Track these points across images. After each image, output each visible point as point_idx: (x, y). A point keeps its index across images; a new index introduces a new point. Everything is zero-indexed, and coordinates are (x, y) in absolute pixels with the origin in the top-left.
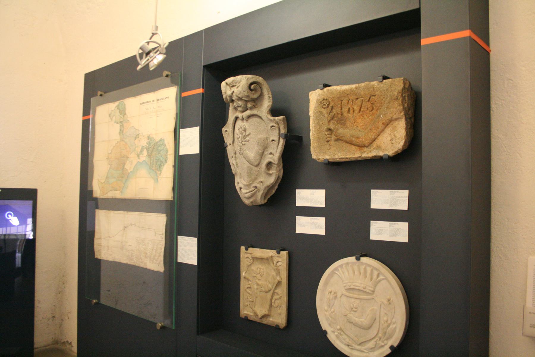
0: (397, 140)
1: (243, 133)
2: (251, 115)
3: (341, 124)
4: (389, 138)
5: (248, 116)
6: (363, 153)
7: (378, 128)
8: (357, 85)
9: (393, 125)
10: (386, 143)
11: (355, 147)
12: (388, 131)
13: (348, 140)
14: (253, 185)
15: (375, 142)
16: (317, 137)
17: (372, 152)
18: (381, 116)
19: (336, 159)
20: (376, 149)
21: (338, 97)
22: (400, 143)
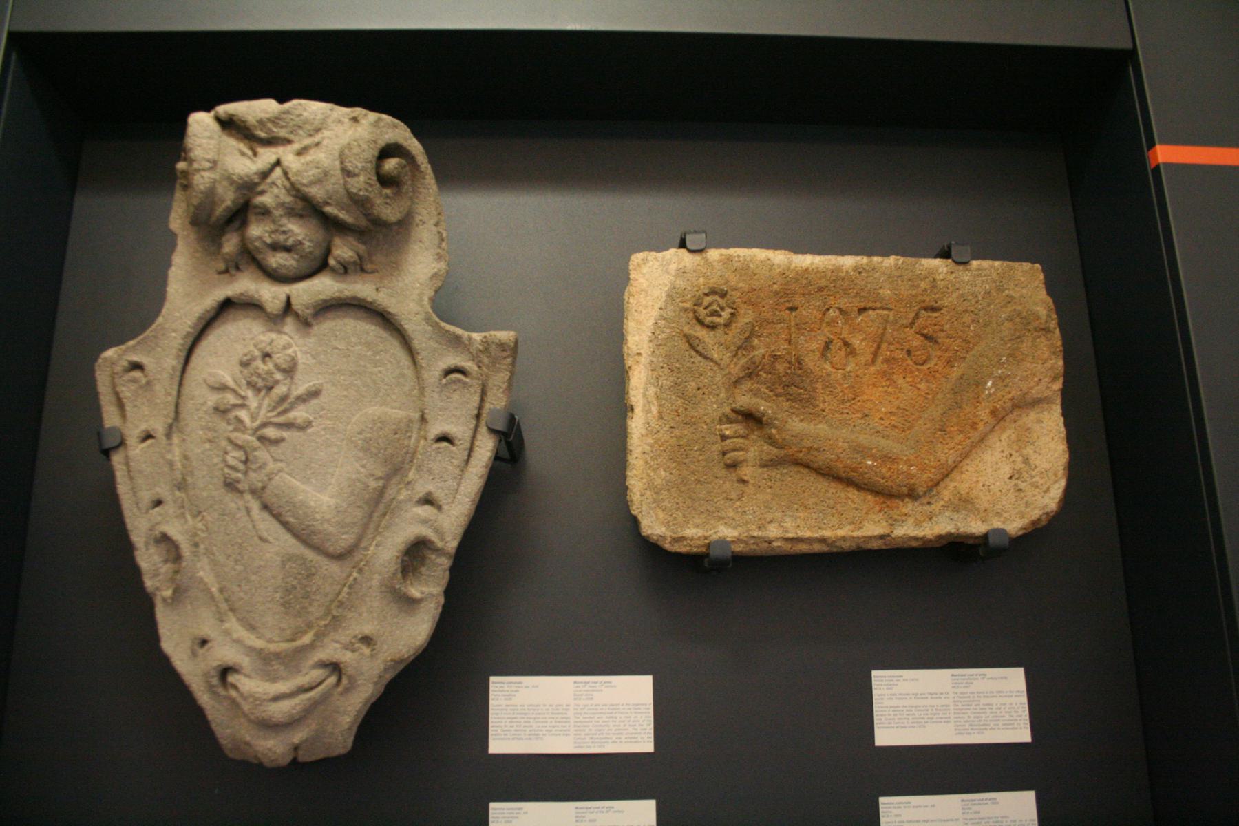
0: (1037, 479)
1: (277, 382)
2: (340, 299)
3: (790, 398)
4: (1006, 470)
5: (325, 301)
6: (895, 520)
7: (974, 426)
8: (863, 260)
9: (1020, 423)
10: (992, 487)
11: (862, 494)
12: (998, 443)
13: (840, 465)
14: (322, 655)
15: (947, 480)
16: (673, 441)
17: (934, 519)
18: (986, 384)
19: (770, 542)
20: (956, 510)
21: (776, 293)
22: (1048, 490)
